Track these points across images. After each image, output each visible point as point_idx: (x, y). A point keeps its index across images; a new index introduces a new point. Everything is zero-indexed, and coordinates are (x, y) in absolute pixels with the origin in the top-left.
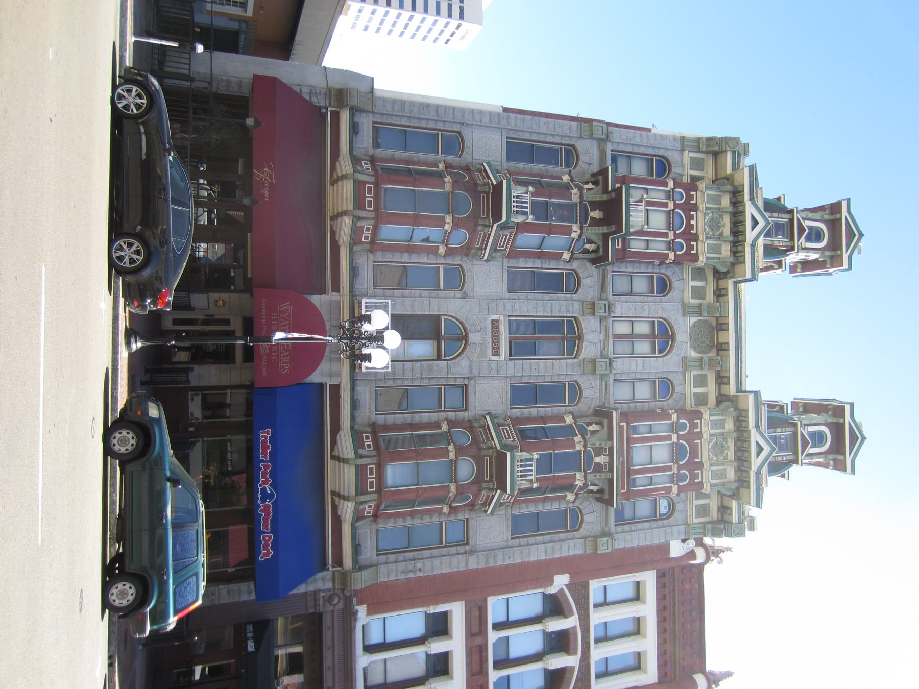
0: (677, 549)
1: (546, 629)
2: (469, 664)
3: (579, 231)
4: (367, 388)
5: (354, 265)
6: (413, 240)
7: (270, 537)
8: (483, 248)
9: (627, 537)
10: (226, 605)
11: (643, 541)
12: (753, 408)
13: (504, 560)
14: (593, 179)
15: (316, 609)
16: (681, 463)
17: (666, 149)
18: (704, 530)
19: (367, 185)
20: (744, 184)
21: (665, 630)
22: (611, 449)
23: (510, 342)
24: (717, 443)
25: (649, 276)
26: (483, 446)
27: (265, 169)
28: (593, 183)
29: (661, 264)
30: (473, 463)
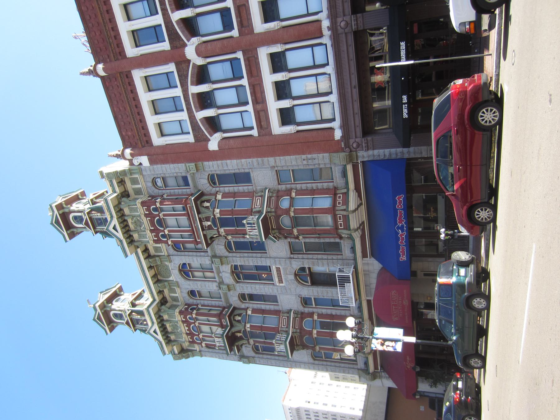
0: (144, 160)
1: (204, 60)
2: (263, 92)
3: (246, 328)
4: (347, 255)
5: (345, 178)
6: (312, 199)
7: (398, 206)
8: (269, 198)
9: (178, 171)
10: (424, 145)
11: (167, 167)
12: (126, 250)
13: (252, 162)
14: (214, 239)
15: (367, 140)
16: (194, 325)
17: (209, 352)
18: (130, 172)
19: (343, 227)
20: (128, 247)
21: (136, 106)
22: (203, 230)
23: (271, 271)
24: (140, 226)
25: (168, 187)
26: (274, 214)
27: (409, 367)
28: (213, 237)
29: (162, 196)
30: (282, 226)
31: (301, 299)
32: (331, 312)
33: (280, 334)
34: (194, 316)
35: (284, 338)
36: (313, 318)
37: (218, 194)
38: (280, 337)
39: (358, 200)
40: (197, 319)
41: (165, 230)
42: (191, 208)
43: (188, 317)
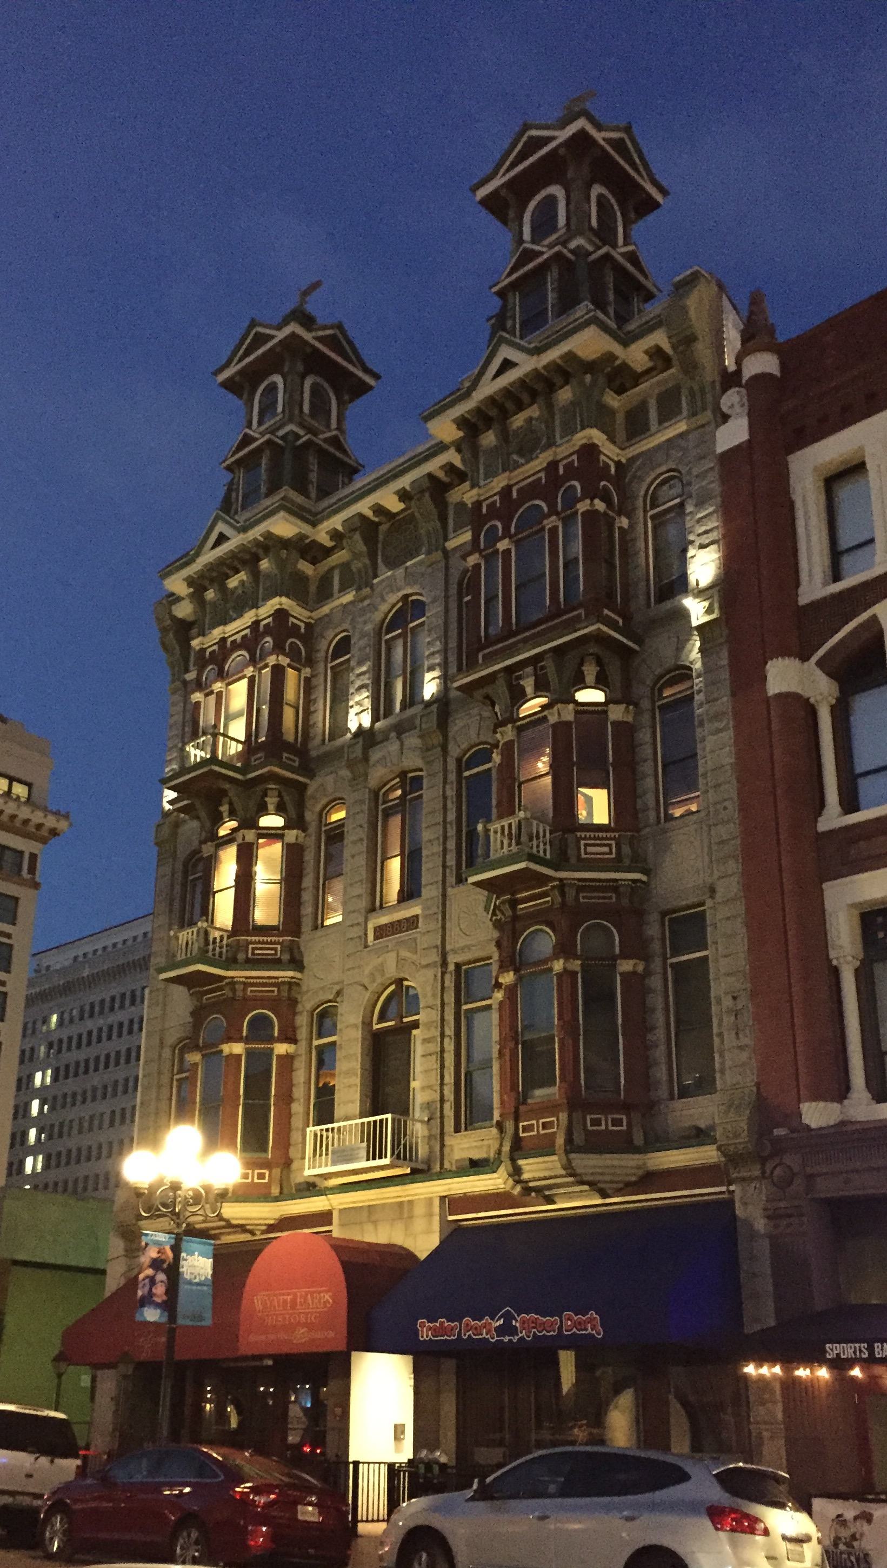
16: (546, 509)
22: (509, 670)
28: (493, 705)
31: (330, 1001)
32: (298, 1100)
33: (551, 834)
34: (582, 507)
35: (538, 852)
36: (625, 956)
37: (627, 708)
38: (541, 834)
39: (616, 1182)
40: (568, 521)
41: (477, 555)
42: (571, 626)
43: (493, 523)
